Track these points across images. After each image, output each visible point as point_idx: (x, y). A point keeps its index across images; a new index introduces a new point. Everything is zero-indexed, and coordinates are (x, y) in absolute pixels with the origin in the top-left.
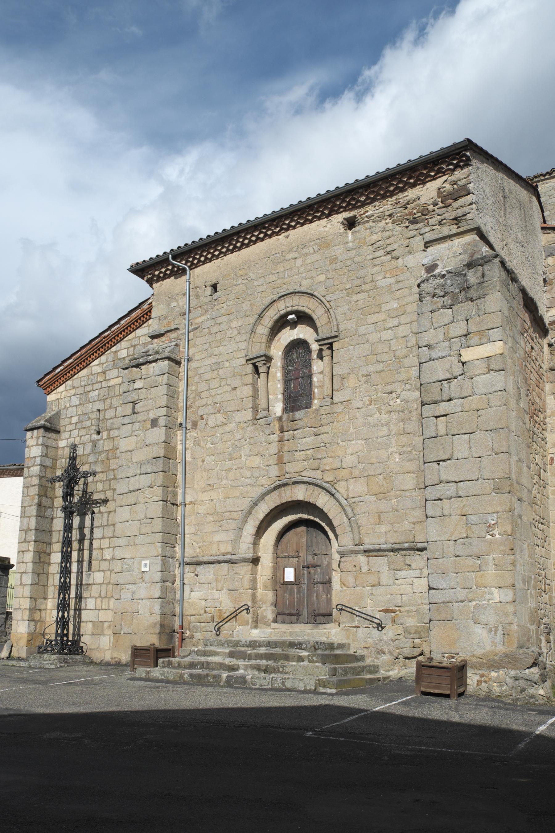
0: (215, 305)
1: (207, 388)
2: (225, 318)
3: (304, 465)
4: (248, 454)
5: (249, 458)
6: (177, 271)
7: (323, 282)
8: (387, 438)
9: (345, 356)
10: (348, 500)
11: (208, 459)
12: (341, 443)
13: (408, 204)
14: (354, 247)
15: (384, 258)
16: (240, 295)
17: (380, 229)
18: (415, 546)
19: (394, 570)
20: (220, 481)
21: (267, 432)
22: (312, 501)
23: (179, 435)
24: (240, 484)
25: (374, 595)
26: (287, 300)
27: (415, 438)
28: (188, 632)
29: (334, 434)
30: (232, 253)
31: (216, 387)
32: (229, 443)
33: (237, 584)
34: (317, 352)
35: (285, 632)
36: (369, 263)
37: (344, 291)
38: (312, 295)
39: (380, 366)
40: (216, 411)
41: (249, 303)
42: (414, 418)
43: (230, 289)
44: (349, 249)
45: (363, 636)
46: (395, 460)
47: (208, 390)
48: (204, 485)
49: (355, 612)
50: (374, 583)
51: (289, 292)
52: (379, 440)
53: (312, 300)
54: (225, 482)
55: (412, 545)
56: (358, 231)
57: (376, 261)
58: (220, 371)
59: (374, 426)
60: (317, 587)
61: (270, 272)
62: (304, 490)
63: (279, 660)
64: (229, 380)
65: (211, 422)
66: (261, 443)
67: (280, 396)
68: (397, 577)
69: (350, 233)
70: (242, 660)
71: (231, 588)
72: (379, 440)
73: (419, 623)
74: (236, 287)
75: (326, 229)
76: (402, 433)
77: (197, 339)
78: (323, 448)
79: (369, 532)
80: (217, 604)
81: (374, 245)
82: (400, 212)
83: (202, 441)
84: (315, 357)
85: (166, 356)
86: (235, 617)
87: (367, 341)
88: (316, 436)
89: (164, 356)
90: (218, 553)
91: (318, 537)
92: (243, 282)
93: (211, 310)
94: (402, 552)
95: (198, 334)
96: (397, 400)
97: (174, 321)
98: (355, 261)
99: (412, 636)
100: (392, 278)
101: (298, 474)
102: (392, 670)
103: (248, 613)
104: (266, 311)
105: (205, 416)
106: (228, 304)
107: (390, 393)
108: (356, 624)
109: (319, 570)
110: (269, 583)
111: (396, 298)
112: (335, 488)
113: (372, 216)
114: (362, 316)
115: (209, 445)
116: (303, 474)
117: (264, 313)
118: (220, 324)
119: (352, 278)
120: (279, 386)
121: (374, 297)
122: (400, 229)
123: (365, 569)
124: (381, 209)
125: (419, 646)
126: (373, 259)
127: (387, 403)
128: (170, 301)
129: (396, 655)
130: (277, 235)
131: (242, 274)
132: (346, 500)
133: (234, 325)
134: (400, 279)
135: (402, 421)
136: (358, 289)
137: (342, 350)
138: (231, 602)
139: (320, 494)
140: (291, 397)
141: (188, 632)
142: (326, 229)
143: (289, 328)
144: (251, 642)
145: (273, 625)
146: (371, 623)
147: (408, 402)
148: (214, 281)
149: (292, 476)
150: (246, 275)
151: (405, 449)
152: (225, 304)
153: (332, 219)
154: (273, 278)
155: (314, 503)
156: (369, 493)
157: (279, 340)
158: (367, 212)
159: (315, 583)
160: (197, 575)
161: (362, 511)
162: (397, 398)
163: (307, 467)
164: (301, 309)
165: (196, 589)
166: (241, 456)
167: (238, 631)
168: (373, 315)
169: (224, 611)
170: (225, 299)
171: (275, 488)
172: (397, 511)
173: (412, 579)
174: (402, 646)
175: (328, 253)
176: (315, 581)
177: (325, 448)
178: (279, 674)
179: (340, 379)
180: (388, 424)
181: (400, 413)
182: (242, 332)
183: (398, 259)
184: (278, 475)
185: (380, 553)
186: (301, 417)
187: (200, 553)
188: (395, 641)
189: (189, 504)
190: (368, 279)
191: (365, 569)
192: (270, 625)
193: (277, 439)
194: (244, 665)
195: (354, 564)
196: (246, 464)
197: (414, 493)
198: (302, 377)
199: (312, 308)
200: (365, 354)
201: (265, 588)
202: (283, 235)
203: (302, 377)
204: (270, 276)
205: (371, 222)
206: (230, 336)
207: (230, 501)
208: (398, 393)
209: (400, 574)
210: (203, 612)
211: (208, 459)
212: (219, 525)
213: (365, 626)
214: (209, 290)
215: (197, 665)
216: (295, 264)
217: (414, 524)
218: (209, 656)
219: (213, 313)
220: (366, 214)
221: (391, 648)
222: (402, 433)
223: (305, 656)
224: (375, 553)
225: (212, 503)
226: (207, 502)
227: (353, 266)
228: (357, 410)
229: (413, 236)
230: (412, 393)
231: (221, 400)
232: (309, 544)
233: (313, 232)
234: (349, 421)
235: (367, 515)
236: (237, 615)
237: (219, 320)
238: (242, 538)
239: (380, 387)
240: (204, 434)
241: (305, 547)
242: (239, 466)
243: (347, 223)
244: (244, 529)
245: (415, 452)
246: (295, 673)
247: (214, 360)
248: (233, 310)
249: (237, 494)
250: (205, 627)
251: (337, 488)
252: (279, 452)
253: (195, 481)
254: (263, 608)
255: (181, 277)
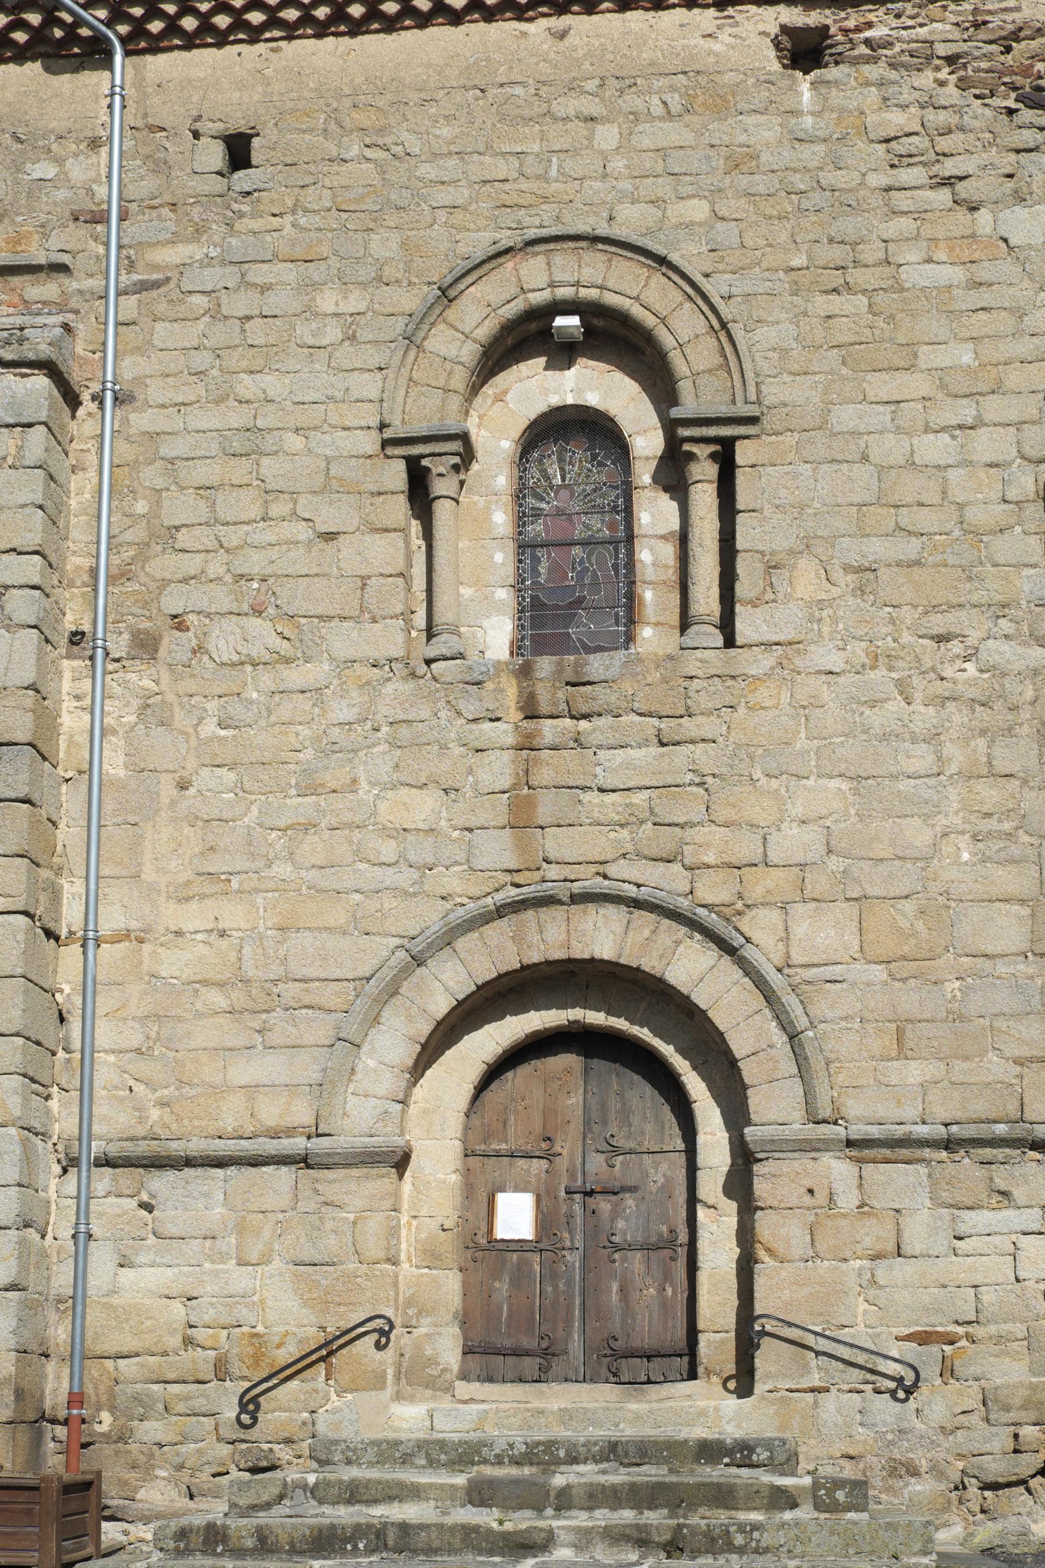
0: (241, 215)
1: (204, 515)
2: (288, 273)
3: (618, 841)
4: (385, 778)
5: (390, 794)
6: (61, 43)
7: (700, 224)
8: (932, 781)
9: (783, 493)
10: (786, 971)
11: (206, 779)
12: (764, 780)
13: (1018, 40)
14: (821, 134)
15: (930, 194)
16: (356, 201)
17: (916, 95)
18: (1030, 1132)
19: (952, 1206)
20: (260, 863)
21: (470, 709)
22: (650, 964)
23: (67, 675)
24: (349, 885)
25: (881, 1287)
26: (558, 259)
27: (1029, 795)
28: (106, 1416)
29: (738, 746)
30: (319, 36)
31: (244, 517)
32: (305, 731)
33: (332, 1240)
34: (653, 465)
35: (541, 1412)
36: (876, 200)
37: (781, 274)
38: (662, 261)
39: (912, 548)
40: (245, 607)
41: (395, 238)
42: (1025, 730)
43: (312, 168)
44: (801, 135)
45: (840, 1420)
46: (959, 857)
47: (207, 524)
48: (187, 875)
49: (810, 1340)
50: (879, 1247)
51: (572, 231)
52: (905, 785)
53: (658, 280)
54: (282, 870)
55: (1019, 1131)
56: (836, 83)
57: (901, 200)
58: (265, 461)
59: (885, 738)
60: (624, 1260)
61: (489, 147)
62: (618, 927)
63: (693, 1507)
64: (302, 500)
65: (222, 643)
66: (444, 747)
67: (504, 595)
68: (963, 1229)
69: (804, 84)
70: (528, 1513)
71: (305, 1257)
72: (905, 785)
73: (1035, 1375)
74: (336, 168)
75: (717, 47)
76: (985, 772)
77: (159, 326)
78: (695, 789)
79: (862, 1082)
80: (243, 1313)
81: (893, 144)
82: (986, 56)
83: (177, 709)
84: (647, 479)
85: (42, 356)
86: (322, 1359)
87: (865, 458)
88: (663, 744)
89: (31, 356)
90: (249, 1129)
91: (628, 1094)
92: (369, 153)
93: (224, 229)
94: (980, 1151)
95: (162, 308)
96: (967, 665)
97: (46, 236)
98: (823, 182)
99: (1013, 1416)
100: (957, 269)
101: (594, 868)
102: (947, 1525)
103: (379, 1346)
104: (469, 279)
105: (192, 619)
106: (302, 221)
107: (941, 639)
108: (815, 1380)
109: (631, 1202)
110: (447, 1244)
111: (968, 335)
112: (737, 929)
113: (888, 45)
114: (845, 371)
115: (210, 727)
116: (612, 870)
117: (461, 286)
118: (265, 289)
119: (813, 237)
120: (499, 557)
121: (892, 317)
122: (987, 112)
123: (848, 1200)
124: (923, 32)
125: (1034, 1447)
126: (888, 189)
127: (933, 669)
128: (22, 152)
129: (956, 1477)
130: (519, 19)
131: (366, 123)
132: (779, 970)
133: (328, 301)
134: (983, 273)
135: (983, 733)
136: (836, 279)
137: (770, 469)
138: (305, 1304)
139: (678, 943)
140: (537, 604)
141: (106, 1416)
142: (710, 44)
143: (542, 361)
144: (531, 1446)
145: (463, 1389)
146: (869, 1377)
147: (1004, 675)
148: (238, 124)
149: (567, 872)
150: (381, 131)
151: (992, 824)
152: (288, 219)
153: (739, 18)
154: (502, 168)
155: (657, 972)
156: (864, 955)
157: (499, 398)
158: (870, 25)
159: (618, 1248)
160: (148, 1207)
161: (839, 1013)
162: (966, 659)
163: (629, 847)
164: (611, 299)
165: (142, 1258)
166: (354, 781)
167: (336, 1411)
168: (884, 376)
169: (277, 1339)
170: (290, 202)
171: (501, 911)
172: (961, 1018)
173: (1014, 1238)
174: (977, 1448)
175: (720, 131)
176: (616, 1239)
177: (701, 791)
178: (734, 1557)
179: (760, 567)
180: (933, 738)
181: (979, 709)
182: (364, 335)
183: (974, 209)
184: (511, 866)
185: (904, 1153)
186: (608, 676)
187: (166, 1126)
188: (952, 1432)
189: (117, 938)
190: (872, 253)
191: (848, 1200)
192: (449, 1389)
193: (510, 740)
194: (578, 1530)
195: (808, 1183)
196: (375, 814)
197: (1021, 967)
198: (584, 543)
199: (657, 307)
200: (857, 499)
201: (431, 1258)
202: (543, 22)
203: (584, 543)
204: (487, 159)
205: (882, 63)
206: (311, 341)
207: (301, 943)
208: (969, 642)
209: (974, 1220)
210: (175, 1341)
211: (206, 779)
212: (257, 1024)
213: (846, 1387)
214: (215, 155)
215: (352, 1539)
216: (590, 138)
217: (1022, 1065)
218: (375, 1501)
219: (234, 241)
220: (868, 34)
221: (940, 1455)
222: (985, 772)
223: (803, 1489)
224: (886, 1152)
225: (224, 943)
226: (200, 937)
227: (817, 198)
228: (824, 677)
229: (1032, 145)
230: (1020, 650)
231: (268, 571)
232: (595, 1116)
233: (663, 43)
234: (792, 711)
235: (857, 1025)
236: (331, 1354)
237: (258, 274)
238: (358, 1077)
239: (907, 614)
240: (190, 685)
241: (576, 1126)
242: (347, 817)
243: (789, 46)
244: (365, 1048)
245: (1026, 839)
246: (799, 1549)
247: (237, 417)
248: (324, 250)
249: (338, 917)
250: (188, 1398)
251: (744, 929)
252: (515, 787)
253: (148, 857)
254: (423, 1330)
255: (76, 70)
